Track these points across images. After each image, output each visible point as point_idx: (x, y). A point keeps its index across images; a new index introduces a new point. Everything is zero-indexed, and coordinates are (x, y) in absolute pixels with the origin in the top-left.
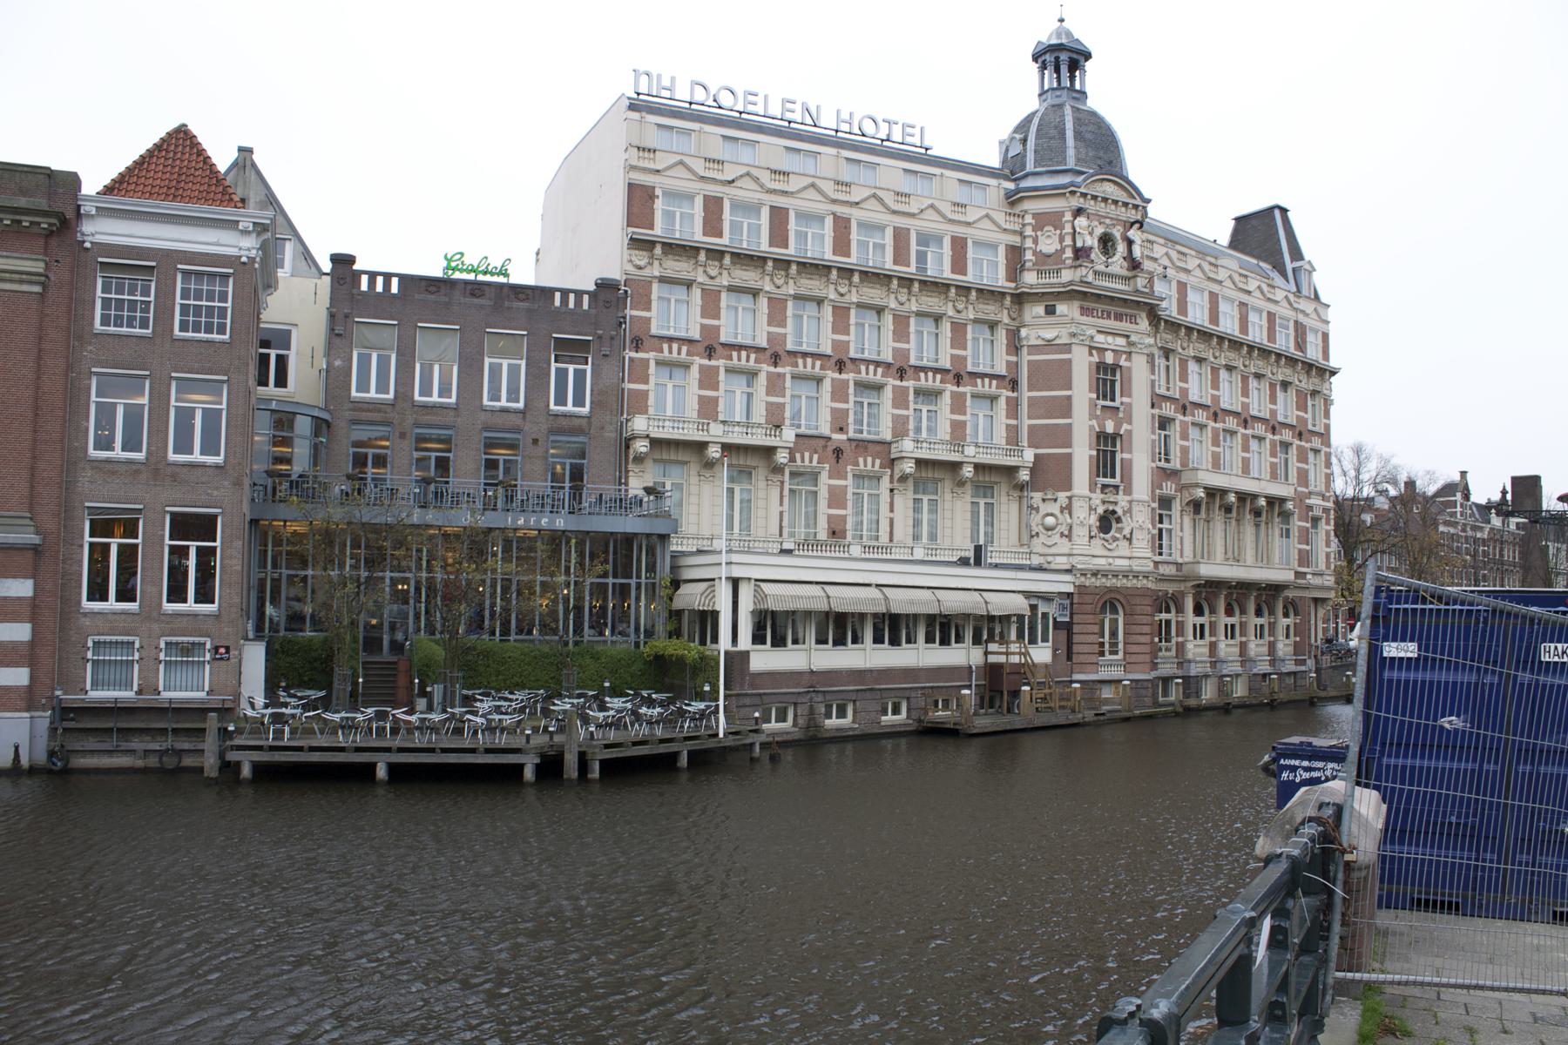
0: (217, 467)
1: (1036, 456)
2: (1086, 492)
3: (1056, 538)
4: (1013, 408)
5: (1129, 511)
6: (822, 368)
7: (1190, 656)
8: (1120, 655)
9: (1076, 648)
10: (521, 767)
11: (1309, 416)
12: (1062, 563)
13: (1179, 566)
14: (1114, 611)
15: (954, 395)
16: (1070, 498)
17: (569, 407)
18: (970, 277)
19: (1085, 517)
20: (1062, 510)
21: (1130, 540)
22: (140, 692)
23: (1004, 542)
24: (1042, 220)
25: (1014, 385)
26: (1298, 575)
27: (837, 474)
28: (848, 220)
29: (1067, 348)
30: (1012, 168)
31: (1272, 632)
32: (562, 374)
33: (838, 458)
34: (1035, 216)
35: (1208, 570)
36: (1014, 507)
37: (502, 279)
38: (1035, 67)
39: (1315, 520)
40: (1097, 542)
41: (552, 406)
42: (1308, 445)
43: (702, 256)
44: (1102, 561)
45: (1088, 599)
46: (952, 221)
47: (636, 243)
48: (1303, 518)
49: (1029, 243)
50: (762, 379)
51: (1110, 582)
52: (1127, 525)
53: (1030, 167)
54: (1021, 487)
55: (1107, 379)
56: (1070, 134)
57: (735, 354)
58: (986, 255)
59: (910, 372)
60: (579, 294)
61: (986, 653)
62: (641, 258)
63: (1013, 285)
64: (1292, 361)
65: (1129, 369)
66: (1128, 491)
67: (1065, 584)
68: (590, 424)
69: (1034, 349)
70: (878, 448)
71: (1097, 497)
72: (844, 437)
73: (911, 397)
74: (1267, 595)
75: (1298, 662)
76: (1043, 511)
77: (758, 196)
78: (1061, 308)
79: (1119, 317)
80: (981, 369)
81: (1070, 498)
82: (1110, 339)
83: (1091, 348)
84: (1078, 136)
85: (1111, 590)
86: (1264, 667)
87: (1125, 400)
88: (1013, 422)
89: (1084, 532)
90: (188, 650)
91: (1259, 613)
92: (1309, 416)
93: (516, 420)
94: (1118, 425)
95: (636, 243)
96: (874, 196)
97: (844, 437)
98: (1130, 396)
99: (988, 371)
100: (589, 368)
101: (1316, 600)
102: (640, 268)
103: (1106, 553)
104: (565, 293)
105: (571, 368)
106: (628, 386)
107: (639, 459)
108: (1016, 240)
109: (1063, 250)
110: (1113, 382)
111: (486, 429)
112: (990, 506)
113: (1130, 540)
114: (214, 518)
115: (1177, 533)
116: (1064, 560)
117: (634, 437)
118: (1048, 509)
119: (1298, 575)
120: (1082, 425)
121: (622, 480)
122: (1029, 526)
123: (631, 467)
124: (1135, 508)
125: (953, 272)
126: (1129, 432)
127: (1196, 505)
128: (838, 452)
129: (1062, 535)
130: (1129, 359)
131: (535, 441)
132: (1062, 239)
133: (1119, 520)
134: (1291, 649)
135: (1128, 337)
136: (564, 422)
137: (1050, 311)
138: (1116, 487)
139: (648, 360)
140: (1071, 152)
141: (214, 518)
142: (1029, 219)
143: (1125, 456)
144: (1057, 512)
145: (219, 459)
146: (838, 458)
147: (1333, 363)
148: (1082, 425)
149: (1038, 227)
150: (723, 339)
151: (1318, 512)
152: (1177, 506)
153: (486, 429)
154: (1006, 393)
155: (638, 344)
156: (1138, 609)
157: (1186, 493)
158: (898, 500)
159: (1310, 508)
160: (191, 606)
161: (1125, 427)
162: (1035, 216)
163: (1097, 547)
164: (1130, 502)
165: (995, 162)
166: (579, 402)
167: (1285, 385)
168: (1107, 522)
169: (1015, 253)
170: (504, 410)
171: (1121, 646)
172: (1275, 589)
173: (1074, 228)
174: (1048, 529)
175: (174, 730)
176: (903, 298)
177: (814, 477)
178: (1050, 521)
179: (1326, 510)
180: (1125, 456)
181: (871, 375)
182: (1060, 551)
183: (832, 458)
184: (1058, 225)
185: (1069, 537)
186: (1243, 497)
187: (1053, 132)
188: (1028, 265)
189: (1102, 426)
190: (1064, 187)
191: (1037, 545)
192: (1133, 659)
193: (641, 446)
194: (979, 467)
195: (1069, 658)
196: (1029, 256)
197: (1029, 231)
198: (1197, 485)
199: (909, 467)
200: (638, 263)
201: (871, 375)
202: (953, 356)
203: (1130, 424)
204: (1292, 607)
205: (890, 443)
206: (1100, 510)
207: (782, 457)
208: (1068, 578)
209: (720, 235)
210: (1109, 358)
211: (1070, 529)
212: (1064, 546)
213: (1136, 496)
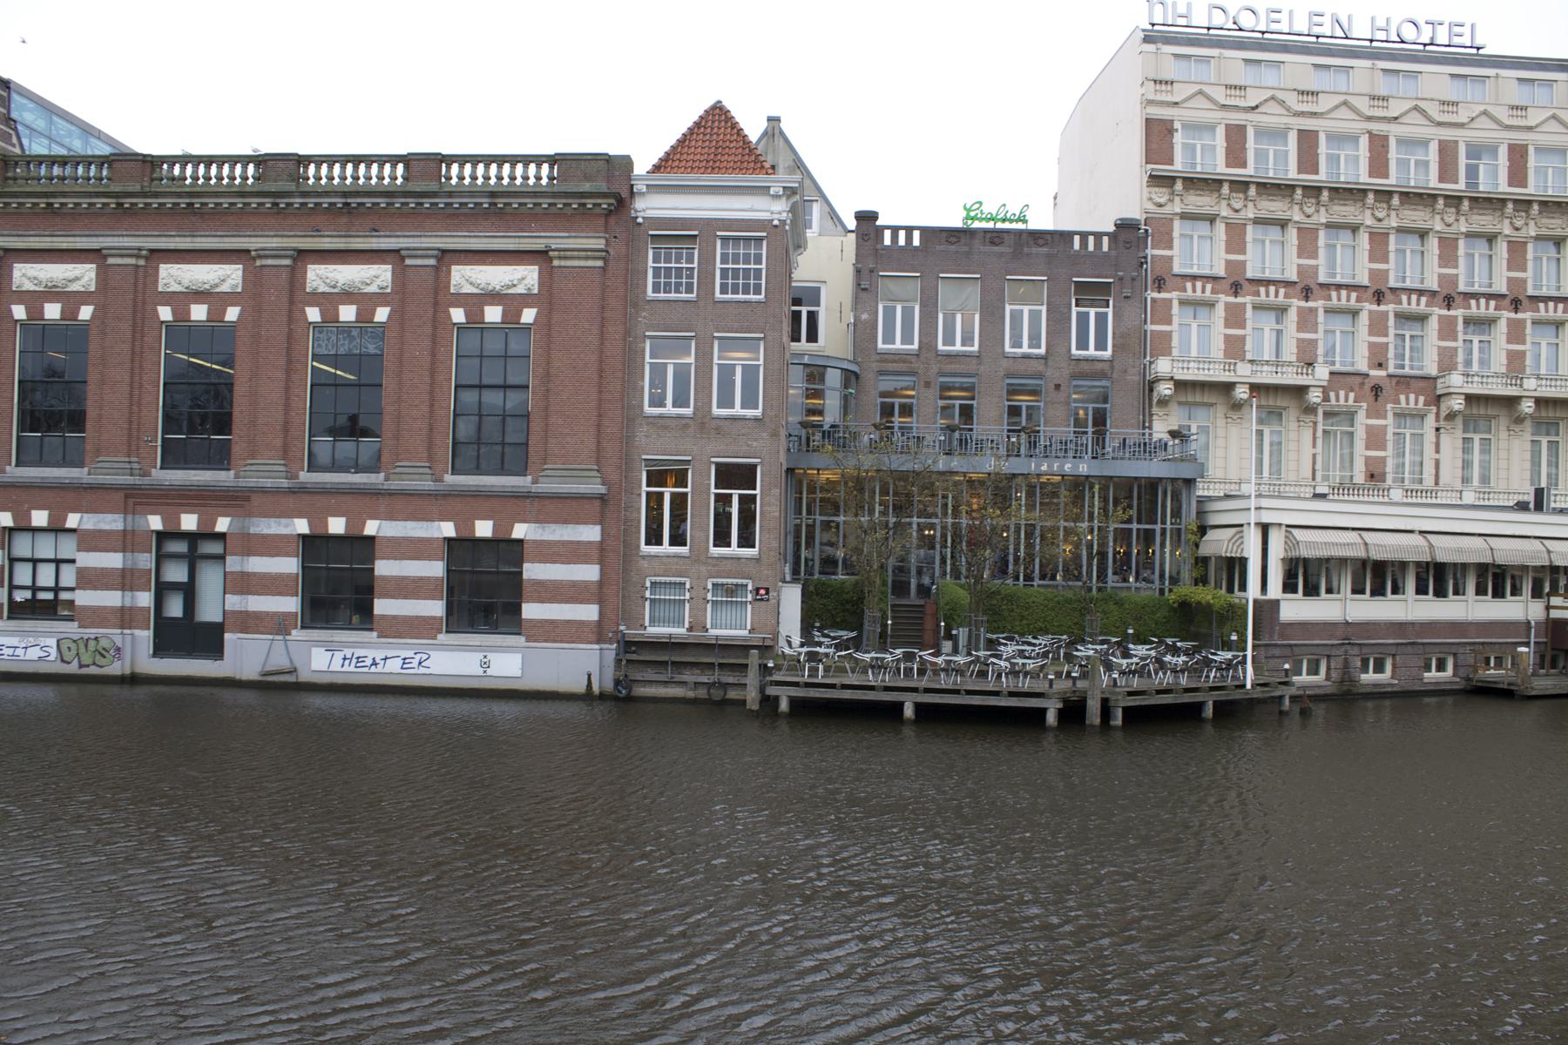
0: (756, 419)
6: (1358, 300)
10: (1043, 711)
17: (1092, 351)
22: (690, 629)
33: (1377, 396)
36: (1307, 435)
37: (1020, 226)
41: (1074, 351)
43: (1226, 189)
60: (1098, 236)
61: (1548, 608)
62: (1161, 195)
68: (1112, 367)
70: (1422, 384)
73: (1460, 327)
90: (732, 591)
93: (1038, 366)
95: (1156, 180)
99: (1554, 293)
100: (1110, 311)
104: (1084, 236)
105: (1092, 312)
107: (1163, 402)
111: (1009, 376)
112: (1553, 445)
117: (1157, 380)
121: (1146, 424)
128: (1377, 390)
131: (1057, 387)
136: (1086, 367)
145: (758, 412)
146: (1377, 396)
150: (1249, 275)
153: (1009, 376)
155: (1160, 284)
170: (1026, 357)
175: (720, 665)
176: (1450, 219)
177: (1350, 416)
181: (1551, 313)
183: (1370, 396)
193: (1165, 389)
199: (1457, 404)
201: (1551, 313)
205: (1435, 379)
207: (1314, 396)
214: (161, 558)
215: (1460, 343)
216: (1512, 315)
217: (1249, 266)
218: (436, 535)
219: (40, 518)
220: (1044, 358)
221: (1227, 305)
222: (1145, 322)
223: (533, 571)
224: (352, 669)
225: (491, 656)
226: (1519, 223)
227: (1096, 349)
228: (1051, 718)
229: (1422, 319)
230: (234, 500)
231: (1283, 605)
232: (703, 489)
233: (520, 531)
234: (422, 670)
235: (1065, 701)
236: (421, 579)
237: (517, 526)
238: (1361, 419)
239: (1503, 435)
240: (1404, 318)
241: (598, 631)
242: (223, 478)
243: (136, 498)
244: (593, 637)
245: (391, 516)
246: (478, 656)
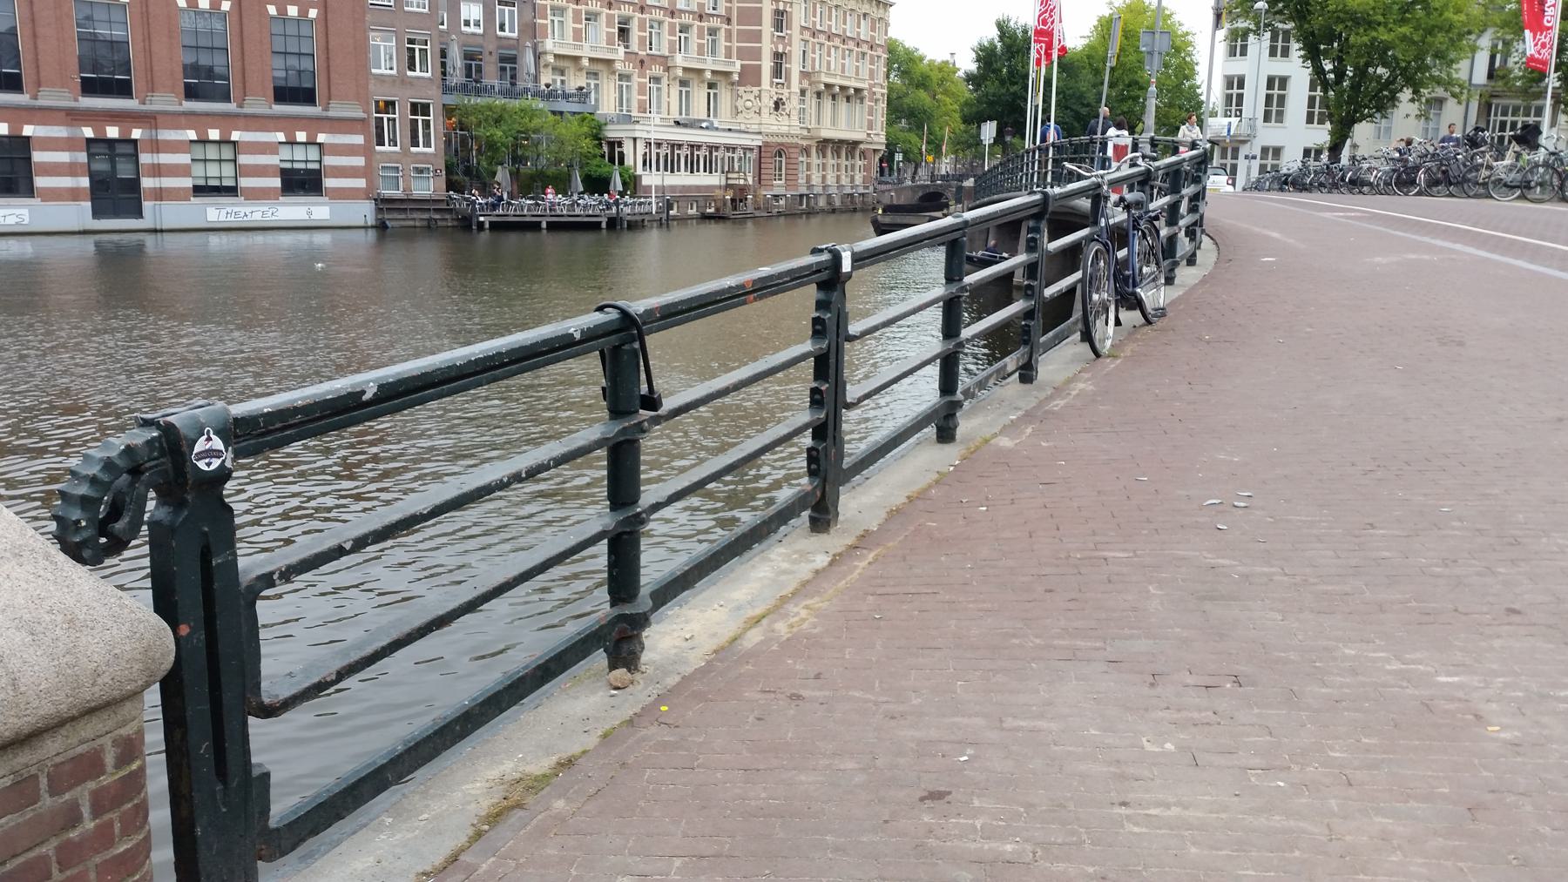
0: (429, 79)
1: (742, 65)
2: (769, 88)
3: (752, 114)
5: (789, 98)
8: (783, 181)
9: (763, 177)
10: (601, 222)
11: (876, 35)
12: (755, 128)
13: (809, 130)
14: (781, 156)
22: (404, 191)
25: (729, 21)
26: (869, 135)
27: (642, 75)
31: (853, 170)
32: (502, 12)
36: (729, 94)
42: (875, 53)
44: (775, 127)
45: (769, 149)
51: (780, 140)
54: (733, 84)
59: (677, 14)
61: (727, 179)
65: (791, 13)
66: (789, 87)
67: (757, 141)
70: (662, 60)
76: (745, 98)
86: (848, 191)
87: (789, 32)
88: (728, 44)
90: (420, 171)
91: (847, 159)
92: (876, 35)
93: (480, 40)
94: (784, 48)
97: (644, 53)
100: (516, 9)
101: (875, 150)
103: (777, 123)
106: (539, 21)
114: (429, 104)
115: (809, 110)
116: (756, 127)
118: (747, 94)
119: (869, 135)
120: (767, 48)
122: (736, 108)
124: (792, 97)
126: (790, 51)
128: (642, 62)
131: (491, 53)
133: (783, 104)
134: (861, 180)
141: (429, 104)
143: (788, 66)
144: (753, 99)
145: (429, 75)
148: (767, 48)
151: (878, 96)
152: (808, 94)
159: (874, 93)
160: (421, 149)
161: (788, 48)
163: (772, 120)
168: (778, 105)
170: (474, 34)
171: (783, 177)
172: (856, 143)
175: (434, 209)
178: (749, 104)
179: (883, 95)
180: (788, 66)
185: (759, 114)
189: (777, 48)
191: (740, 118)
198: (820, 82)
204: (863, 154)
208: (760, 137)
212: (756, 119)
213: (792, 90)
214: (91, 156)
218: (79, 135)
219: (301, 136)
220: (482, 35)
223: (38, 156)
224: (233, 219)
225: (312, 208)
228: (604, 225)
229: (660, 23)
230: (149, 119)
231: (643, 177)
232: (401, 114)
233: (28, 130)
234: (274, 218)
236: (267, 165)
237: (234, 133)
238: (636, 79)
241: (366, 194)
242: (231, 107)
243: (75, 116)
244: (364, 196)
245: (247, 129)
246: (305, 209)
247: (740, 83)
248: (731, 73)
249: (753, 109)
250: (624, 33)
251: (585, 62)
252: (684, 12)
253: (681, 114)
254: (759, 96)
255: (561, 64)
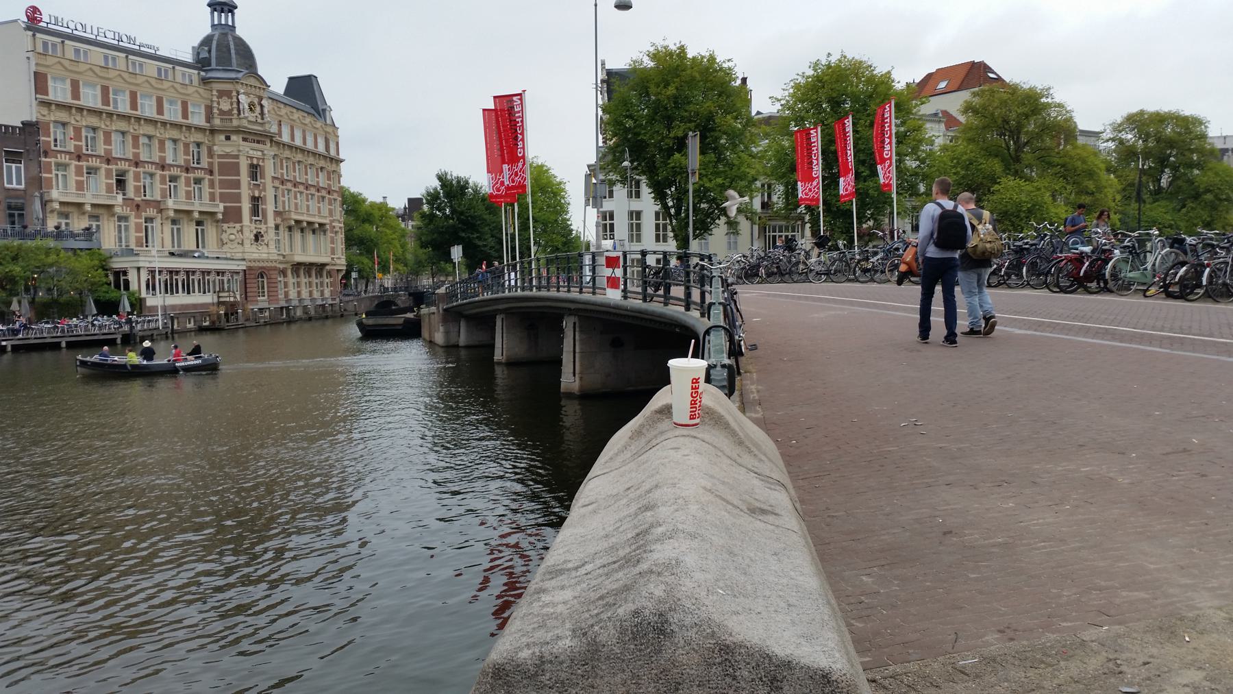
1: (225, 207)
3: (236, 245)
4: (212, 185)
5: (267, 232)
6: (129, 166)
7: (291, 297)
8: (266, 297)
9: (248, 294)
12: (239, 256)
14: (262, 277)
15: (77, 167)
16: (242, 227)
17: (14, 186)
18: (82, 103)
19: (249, 235)
20: (238, 232)
21: (267, 245)
23: (210, 247)
24: (222, 94)
25: (211, 173)
26: (333, 259)
28: (108, 87)
29: (237, 157)
30: (201, 63)
31: (298, 286)
32: (9, 169)
33: (138, 209)
34: (218, 91)
35: (299, 258)
36: (214, 230)
38: (209, 9)
39: (336, 232)
40: (254, 246)
44: (257, 255)
45: (253, 272)
46: (181, 93)
47: (44, 104)
48: (332, 232)
49: (215, 105)
50: (158, 178)
51: (261, 264)
52: (266, 238)
53: (214, 66)
54: (217, 221)
55: (255, 171)
56: (233, 51)
57: (90, 159)
58: (59, 85)
59: (167, 167)
61: (219, 297)
62: (45, 111)
63: (208, 125)
64: (325, 157)
65: (264, 166)
67: (242, 266)
68: (25, 193)
69: (220, 156)
71: (253, 225)
72: (139, 199)
73: (53, 167)
74: (318, 269)
75: (333, 299)
77: (123, 85)
78: (234, 137)
79: (258, 142)
80: (118, 156)
81: (242, 227)
82: (255, 152)
83: (248, 157)
84: (237, 53)
85: (261, 268)
86: (319, 302)
87: (263, 181)
89: (248, 242)
94: (260, 193)
96: (91, 69)
97: (139, 199)
98: (264, 179)
99: (122, 157)
100: (22, 166)
101: (338, 270)
102: (44, 116)
105: (14, 166)
106: (44, 175)
108: (208, 103)
109: (232, 110)
110: (256, 172)
112: (178, 230)
113: (267, 245)
116: (240, 255)
117: (51, 201)
118: (231, 230)
119: (333, 259)
120: (245, 193)
123: (48, 215)
124: (270, 230)
125: (103, 105)
126: (265, 196)
127: (290, 228)
128: (138, 206)
129: (238, 243)
130: (263, 162)
132: (232, 104)
133: (262, 236)
134: (329, 294)
135: (262, 151)
136: (12, 193)
137: (228, 138)
138: (261, 221)
139: (51, 162)
140: (234, 61)
142: (215, 93)
143: (264, 207)
146: (138, 209)
147: (341, 156)
148: (245, 193)
149: (220, 97)
151: (337, 229)
152: (281, 228)
154: (208, 177)
155: (46, 154)
156: (273, 277)
157: (285, 222)
158: (165, 228)
159: (334, 227)
161: (263, 193)
162: (218, 91)
164: (267, 228)
165: (188, 57)
166: (19, 183)
167: (322, 168)
168: (257, 237)
169: (209, 109)
171: (266, 293)
173: (238, 99)
174: (231, 241)
176: (108, 123)
178: (232, 237)
179: (340, 228)
180: (264, 207)
181: (94, 163)
182: (237, 251)
183: (135, 209)
184: (230, 97)
185: (242, 244)
186: (309, 223)
187: (225, 49)
188: (216, 115)
189: (253, 193)
190: (233, 79)
192: (271, 298)
194: (93, 205)
195: (246, 299)
196: (215, 111)
197: (215, 99)
200: (43, 113)
201: (94, 163)
202: (133, 153)
203: (265, 191)
206: (255, 232)
208: (244, 263)
209: (137, 110)
210: (255, 162)
211: (243, 241)
212: (240, 248)
213: (269, 225)
215: (53, 176)
216: (77, 163)
217: (113, 152)
221: (134, 172)
222: (41, 172)
226: (136, 127)
227: (17, 184)
235: (123, 335)
238: (133, 221)
239: (186, 226)
240: (58, 165)
247: (224, 221)
248: (192, 211)
249: (237, 241)
250: (121, 183)
251: (88, 208)
252: (121, 159)
253: (173, 247)
254: (241, 231)
255: (66, 209)
